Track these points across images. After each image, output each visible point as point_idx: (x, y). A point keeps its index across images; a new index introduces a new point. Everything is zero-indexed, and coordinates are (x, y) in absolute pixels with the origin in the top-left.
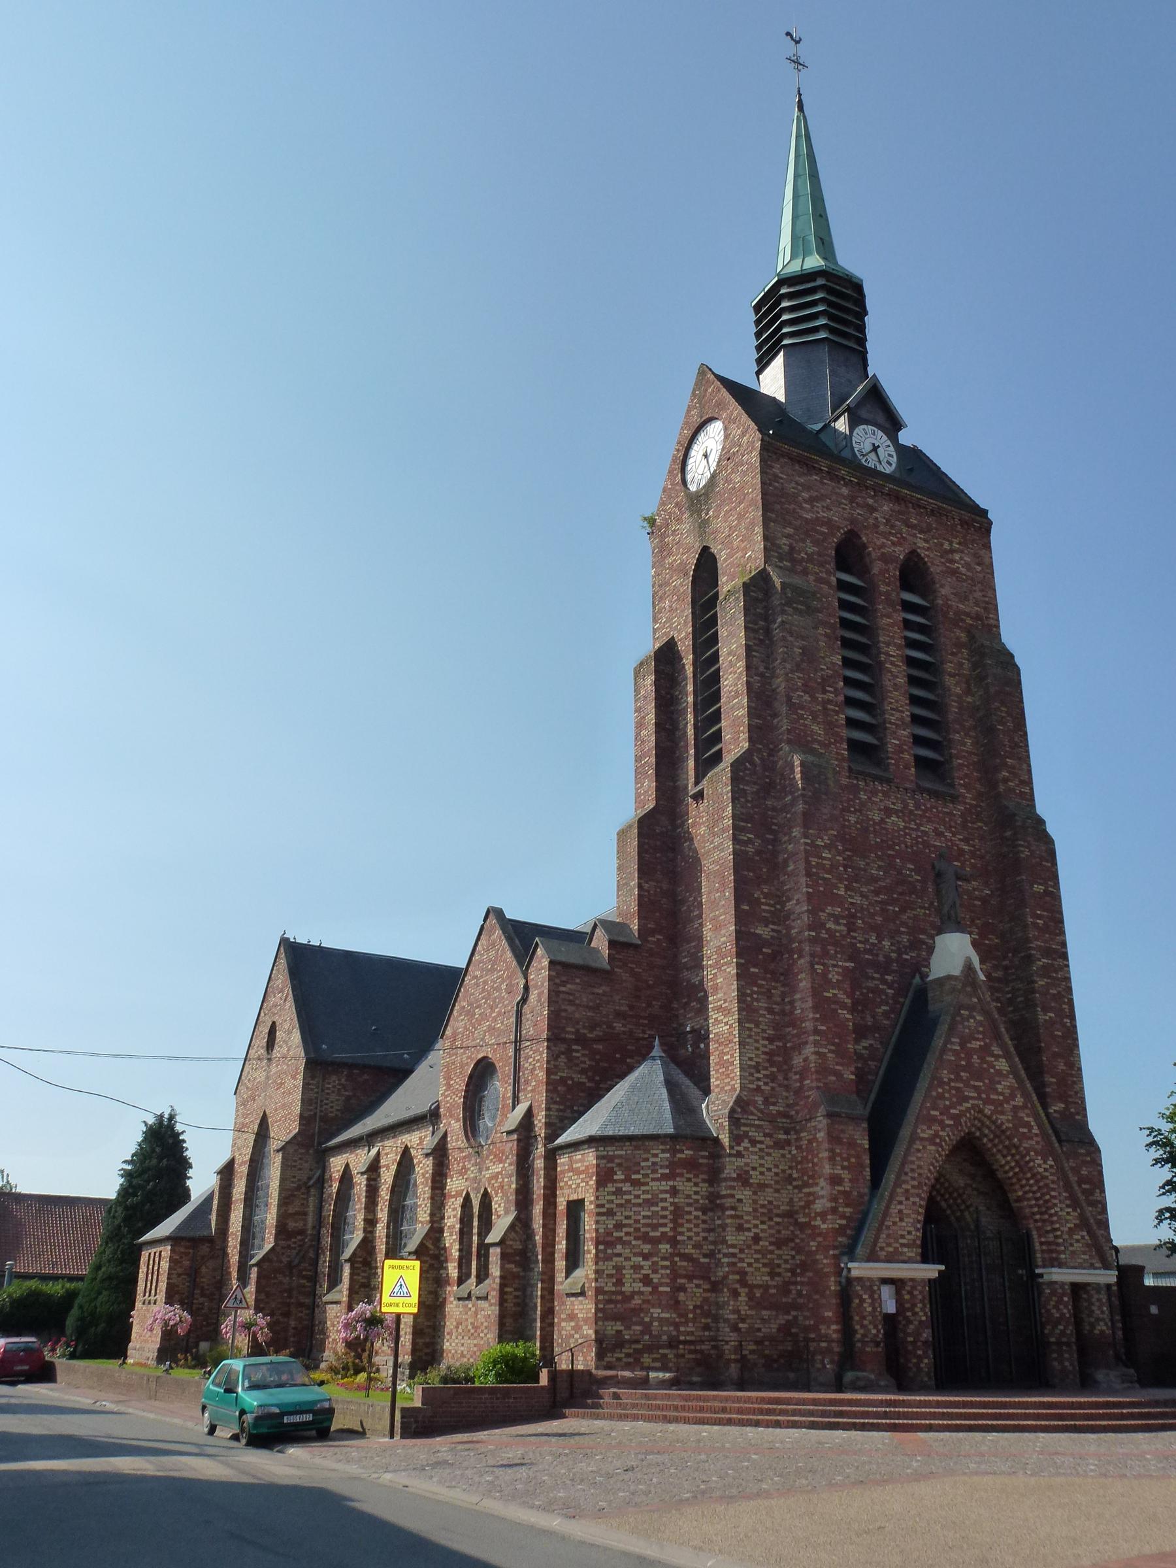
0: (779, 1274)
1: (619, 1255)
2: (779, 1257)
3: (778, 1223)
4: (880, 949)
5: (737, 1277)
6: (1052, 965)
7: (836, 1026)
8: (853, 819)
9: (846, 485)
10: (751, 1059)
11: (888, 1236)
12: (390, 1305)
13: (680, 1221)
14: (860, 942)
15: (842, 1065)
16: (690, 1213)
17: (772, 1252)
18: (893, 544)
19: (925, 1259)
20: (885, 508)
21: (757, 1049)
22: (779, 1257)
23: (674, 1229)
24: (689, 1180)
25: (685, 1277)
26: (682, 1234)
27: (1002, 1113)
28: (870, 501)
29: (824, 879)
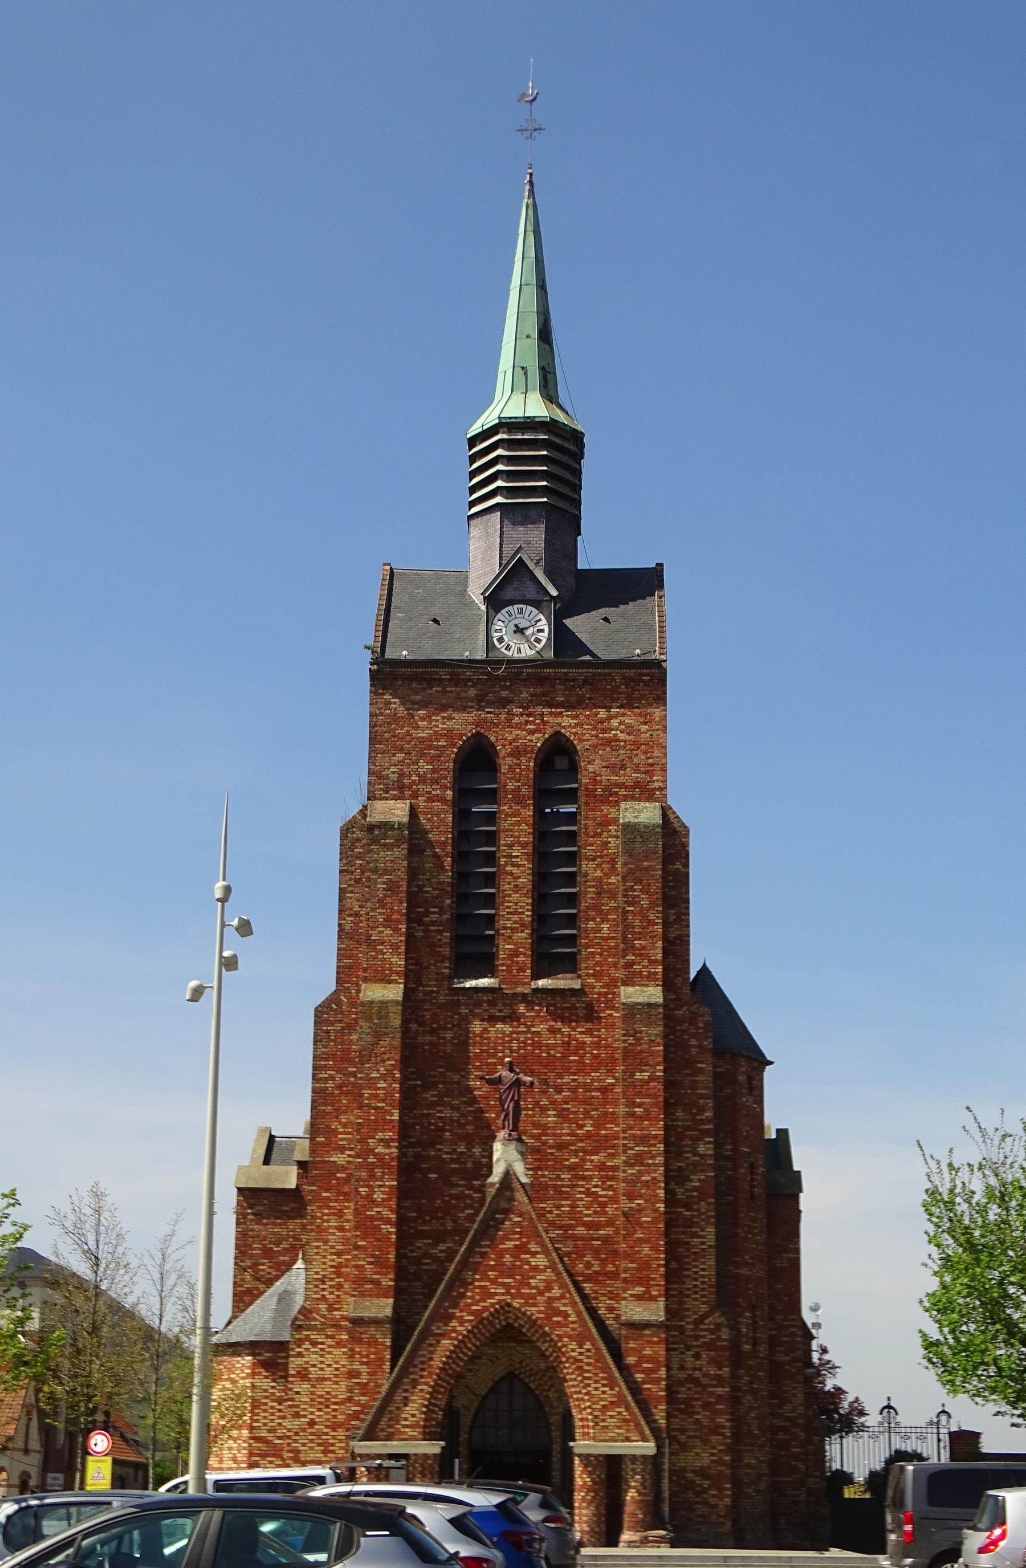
0: (333, 1452)
2: (334, 1438)
3: (335, 1410)
4: (471, 1157)
5: (291, 1455)
6: (650, 1152)
7: (377, 1240)
9: (474, 685)
10: (317, 1273)
11: (390, 1419)
12: (92, 1485)
13: (256, 1411)
14: (447, 1153)
15: (379, 1273)
16: (266, 1404)
17: (326, 1434)
19: (428, 1436)
20: (524, 695)
21: (324, 1263)
22: (334, 1438)
23: (251, 1418)
24: (266, 1377)
25: (258, 1455)
26: (257, 1421)
27: (534, 1305)
28: (504, 694)
29: (378, 1108)
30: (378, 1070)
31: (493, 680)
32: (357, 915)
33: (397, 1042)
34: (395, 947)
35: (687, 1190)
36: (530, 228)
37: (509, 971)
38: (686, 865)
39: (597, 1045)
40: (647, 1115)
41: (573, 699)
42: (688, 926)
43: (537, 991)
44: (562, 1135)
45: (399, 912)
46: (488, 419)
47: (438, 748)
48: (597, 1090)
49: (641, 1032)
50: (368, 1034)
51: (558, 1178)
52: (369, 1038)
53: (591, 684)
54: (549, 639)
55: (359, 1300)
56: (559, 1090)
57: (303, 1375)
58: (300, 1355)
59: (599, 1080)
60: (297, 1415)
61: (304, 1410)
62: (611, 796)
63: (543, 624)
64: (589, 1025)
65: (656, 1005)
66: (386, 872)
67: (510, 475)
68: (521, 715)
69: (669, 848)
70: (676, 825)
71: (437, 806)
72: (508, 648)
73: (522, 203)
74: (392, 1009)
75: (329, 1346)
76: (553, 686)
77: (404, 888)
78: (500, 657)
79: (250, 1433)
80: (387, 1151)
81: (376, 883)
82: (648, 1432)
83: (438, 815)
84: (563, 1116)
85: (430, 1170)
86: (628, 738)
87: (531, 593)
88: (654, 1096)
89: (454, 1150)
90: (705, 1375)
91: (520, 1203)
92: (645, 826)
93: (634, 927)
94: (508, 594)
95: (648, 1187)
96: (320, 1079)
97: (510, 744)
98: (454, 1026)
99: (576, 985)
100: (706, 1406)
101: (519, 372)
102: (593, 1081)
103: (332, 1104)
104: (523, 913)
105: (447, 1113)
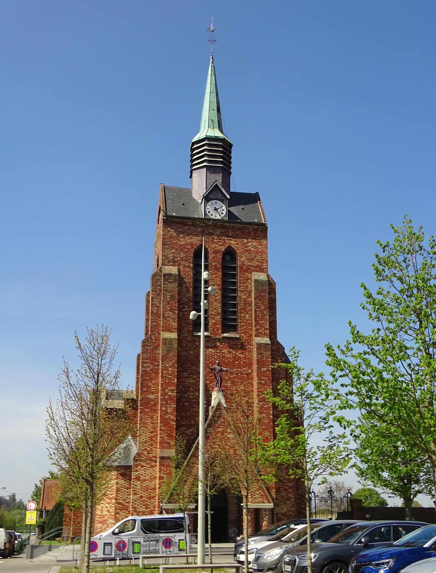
0: (149, 508)
1: (102, 503)
2: (150, 502)
3: (150, 492)
8: (192, 352)
9: (200, 227)
10: (143, 440)
14: (191, 396)
16: (122, 490)
17: (147, 501)
18: (220, 245)
21: (146, 436)
22: (150, 502)
23: (116, 495)
24: (122, 479)
25: (119, 509)
26: (119, 496)
28: (211, 231)
29: (168, 378)
30: (169, 364)
31: (206, 226)
32: (158, 307)
33: (176, 354)
34: (174, 319)
35: (277, 411)
36: (213, 73)
37: (213, 330)
38: (275, 296)
39: (245, 358)
40: (266, 384)
41: (235, 235)
42: (276, 317)
43: (224, 337)
44: (233, 390)
45: (175, 306)
46: (201, 135)
47: (187, 248)
48: (245, 374)
49: (263, 354)
50: (165, 350)
51: (232, 405)
52: (166, 352)
53: (241, 230)
54: (226, 213)
55: (162, 450)
56: (232, 374)
57: (138, 478)
58: (137, 471)
59: (246, 371)
60: (135, 494)
61: (139, 492)
62: (249, 270)
63: (224, 208)
64: (242, 351)
65: (268, 344)
66: (170, 291)
67: (209, 156)
68: (217, 239)
69: (269, 290)
70: (271, 281)
71: (187, 269)
72: (212, 215)
73: (209, 66)
74: (174, 342)
75: (148, 467)
76: (228, 230)
77: (177, 298)
78: (209, 218)
79: (116, 501)
80: (172, 394)
81: (166, 295)
82: (271, 500)
83: (188, 272)
84: (233, 383)
85: (185, 402)
86: (254, 250)
87: (220, 196)
88: (268, 377)
89: (194, 395)
90: (284, 479)
91: (223, 414)
92: (263, 281)
93: (259, 316)
94: (212, 196)
95: (266, 410)
96: (144, 367)
97: (213, 249)
98: (194, 349)
99: (238, 336)
100: (285, 490)
101: (211, 121)
102: (244, 371)
103: (149, 376)
104: (218, 309)
105: (192, 381)
